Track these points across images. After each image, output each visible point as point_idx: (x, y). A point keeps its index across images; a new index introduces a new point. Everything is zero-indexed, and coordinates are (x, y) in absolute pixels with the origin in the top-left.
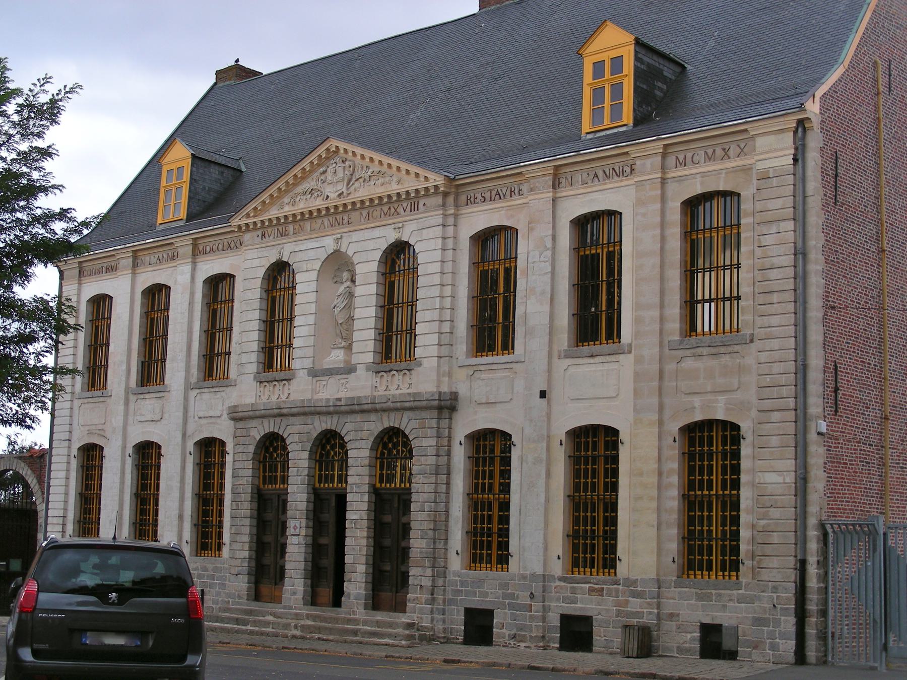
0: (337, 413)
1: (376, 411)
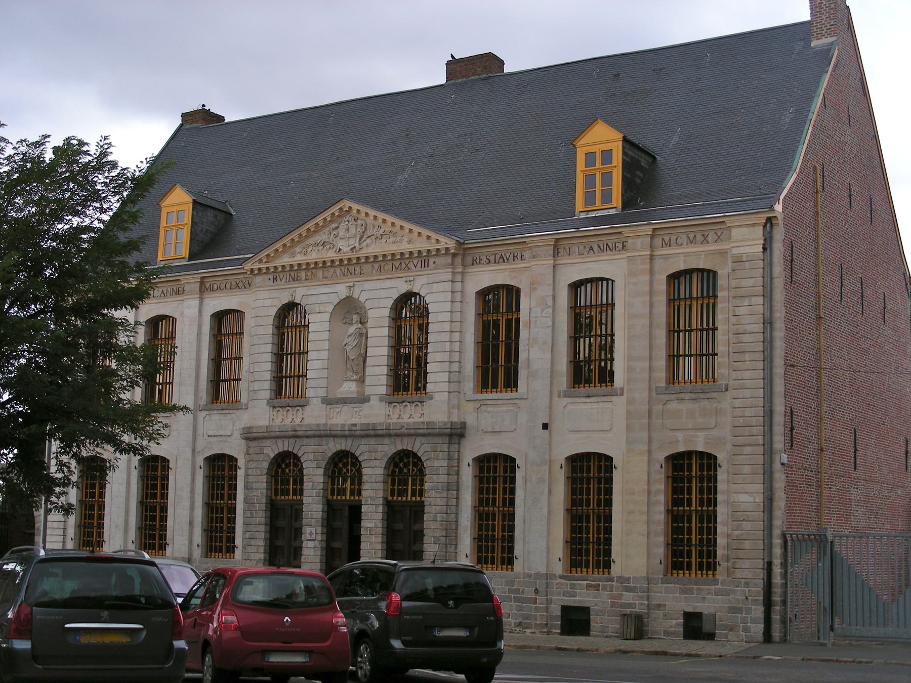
0: (351, 436)
1: (390, 435)
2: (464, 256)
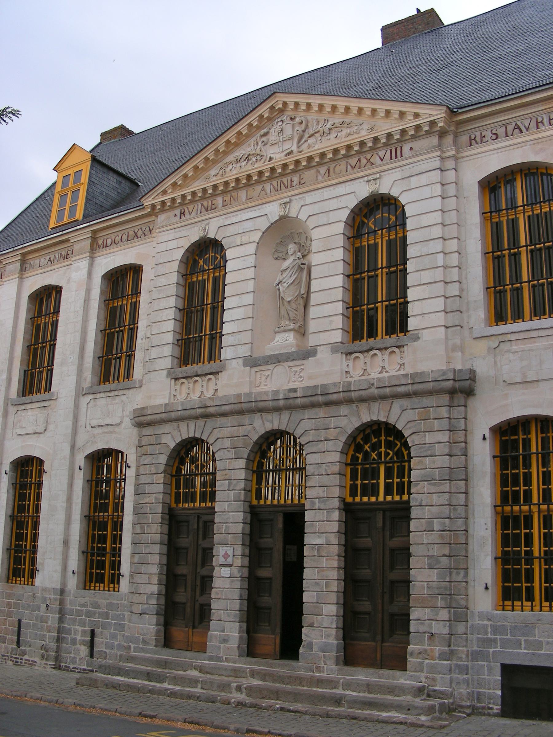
0: (289, 408)
1: (350, 401)
2: (456, 136)
